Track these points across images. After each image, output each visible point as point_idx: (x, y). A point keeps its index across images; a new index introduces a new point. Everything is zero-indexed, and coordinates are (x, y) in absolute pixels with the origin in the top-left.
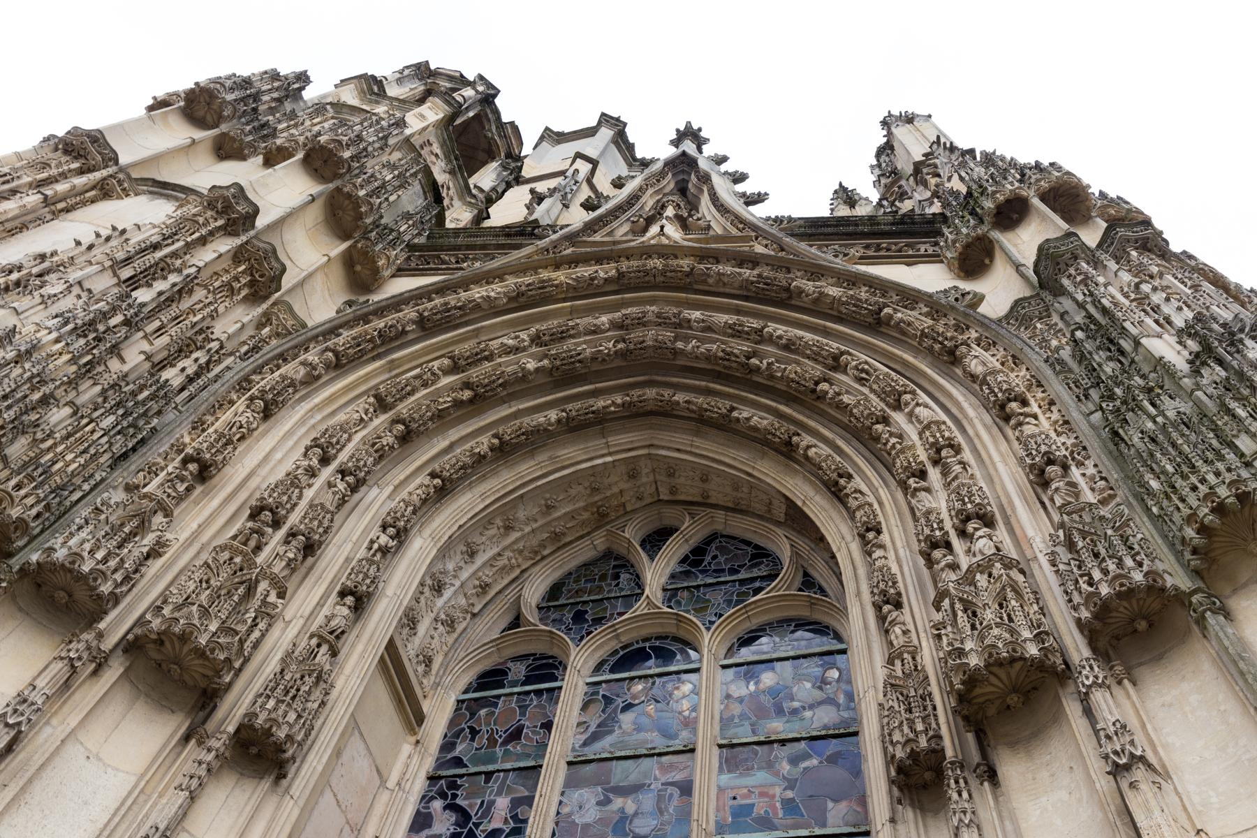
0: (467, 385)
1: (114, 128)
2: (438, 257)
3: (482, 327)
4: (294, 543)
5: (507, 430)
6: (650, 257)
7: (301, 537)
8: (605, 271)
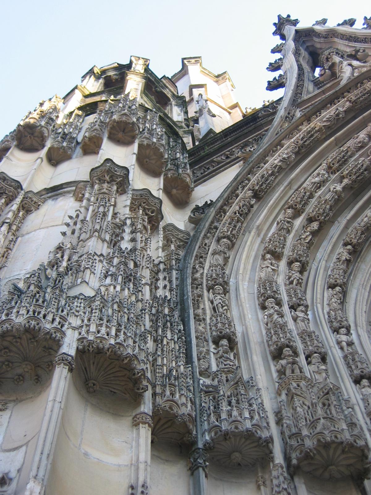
0: (310, 220)
1: (189, 78)
2: (213, 161)
3: (292, 180)
4: (314, 361)
5: (353, 235)
6: (362, 83)
7: (316, 355)
8: (342, 105)
